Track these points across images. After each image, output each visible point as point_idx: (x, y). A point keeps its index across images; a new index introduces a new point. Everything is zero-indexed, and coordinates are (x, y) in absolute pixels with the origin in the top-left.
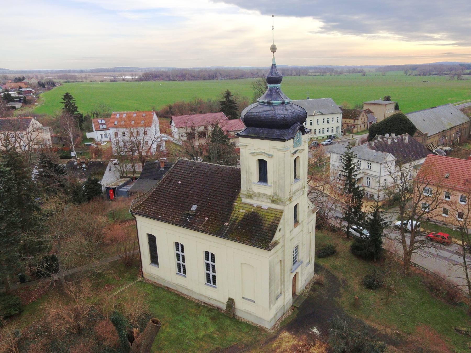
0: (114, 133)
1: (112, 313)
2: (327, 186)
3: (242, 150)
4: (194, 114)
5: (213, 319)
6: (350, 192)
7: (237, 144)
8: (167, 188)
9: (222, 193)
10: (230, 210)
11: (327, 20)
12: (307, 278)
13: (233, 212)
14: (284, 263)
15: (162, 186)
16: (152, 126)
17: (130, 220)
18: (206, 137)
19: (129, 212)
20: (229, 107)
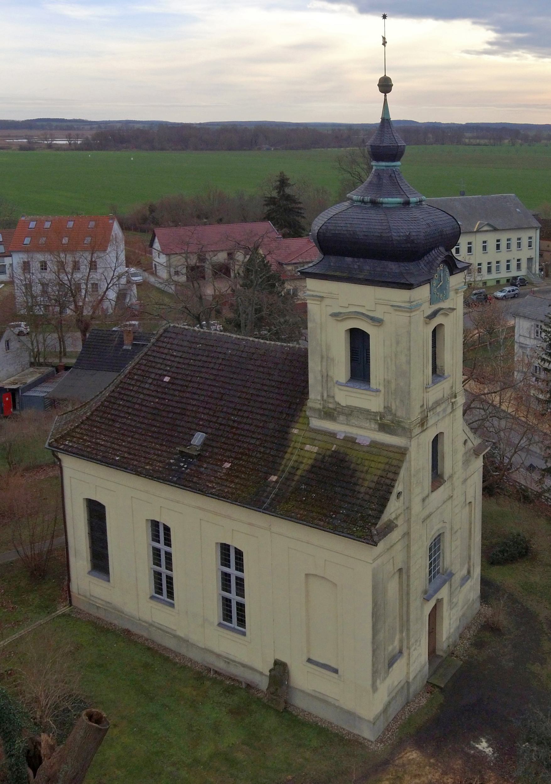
2: (509, 393)
3: (313, 307)
4: (205, 224)
5: (235, 712)
7: (301, 294)
8: (137, 392)
9: (265, 406)
11: (502, 27)
12: (463, 615)
13: (290, 450)
14: (408, 577)
15: (126, 386)
17: (48, 465)
18: (230, 276)
19: (46, 445)
20: (285, 212)
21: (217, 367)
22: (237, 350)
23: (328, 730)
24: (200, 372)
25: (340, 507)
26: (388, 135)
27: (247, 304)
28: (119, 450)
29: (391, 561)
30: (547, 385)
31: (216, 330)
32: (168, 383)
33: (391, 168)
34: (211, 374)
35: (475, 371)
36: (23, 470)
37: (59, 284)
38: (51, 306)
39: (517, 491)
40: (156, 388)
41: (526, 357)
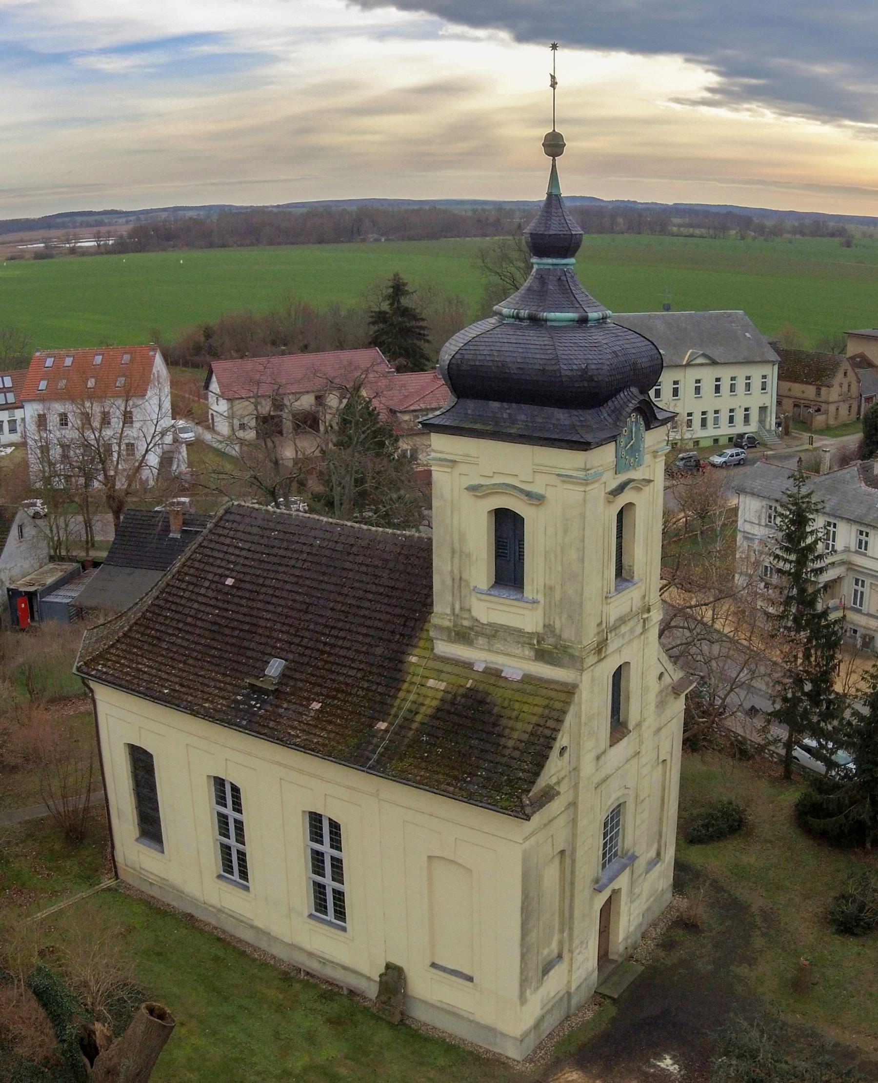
0: (35, 419)
1: (33, 970)
2: (726, 606)
3: (440, 476)
4: (283, 353)
5: (335, 1022)
6: (799, 628)
7: (422, 457)
8: (189, 599)
9: (369, 623)
10: (395, 679)
11: (729, 69)
12: (648, 909)
13: (405, 686)
14: (573, 861)
15: (174, 591)
16: (149, 394)
17: (77, 697)
18: (318, 430)
19: (74, 670)
20: (400, 333)
21: (299, 564)
22: (329, 540)
23: (459, 1047)
24: (277, 572)
25: (477, 767)
26: (557, 219)
27: (343, 472)
28: (168, 680)
29: (550, 840)
30: (781, 593)
31: (298, 510)
32: (232, 587)
33: (561, 267)
34: (292, 575)
35: (678, 573)
36: (48, 702)
37: (83, 445)
38: (74, 476)
39: (732, 744)
40: (214, 594)
41: (752, 553)
